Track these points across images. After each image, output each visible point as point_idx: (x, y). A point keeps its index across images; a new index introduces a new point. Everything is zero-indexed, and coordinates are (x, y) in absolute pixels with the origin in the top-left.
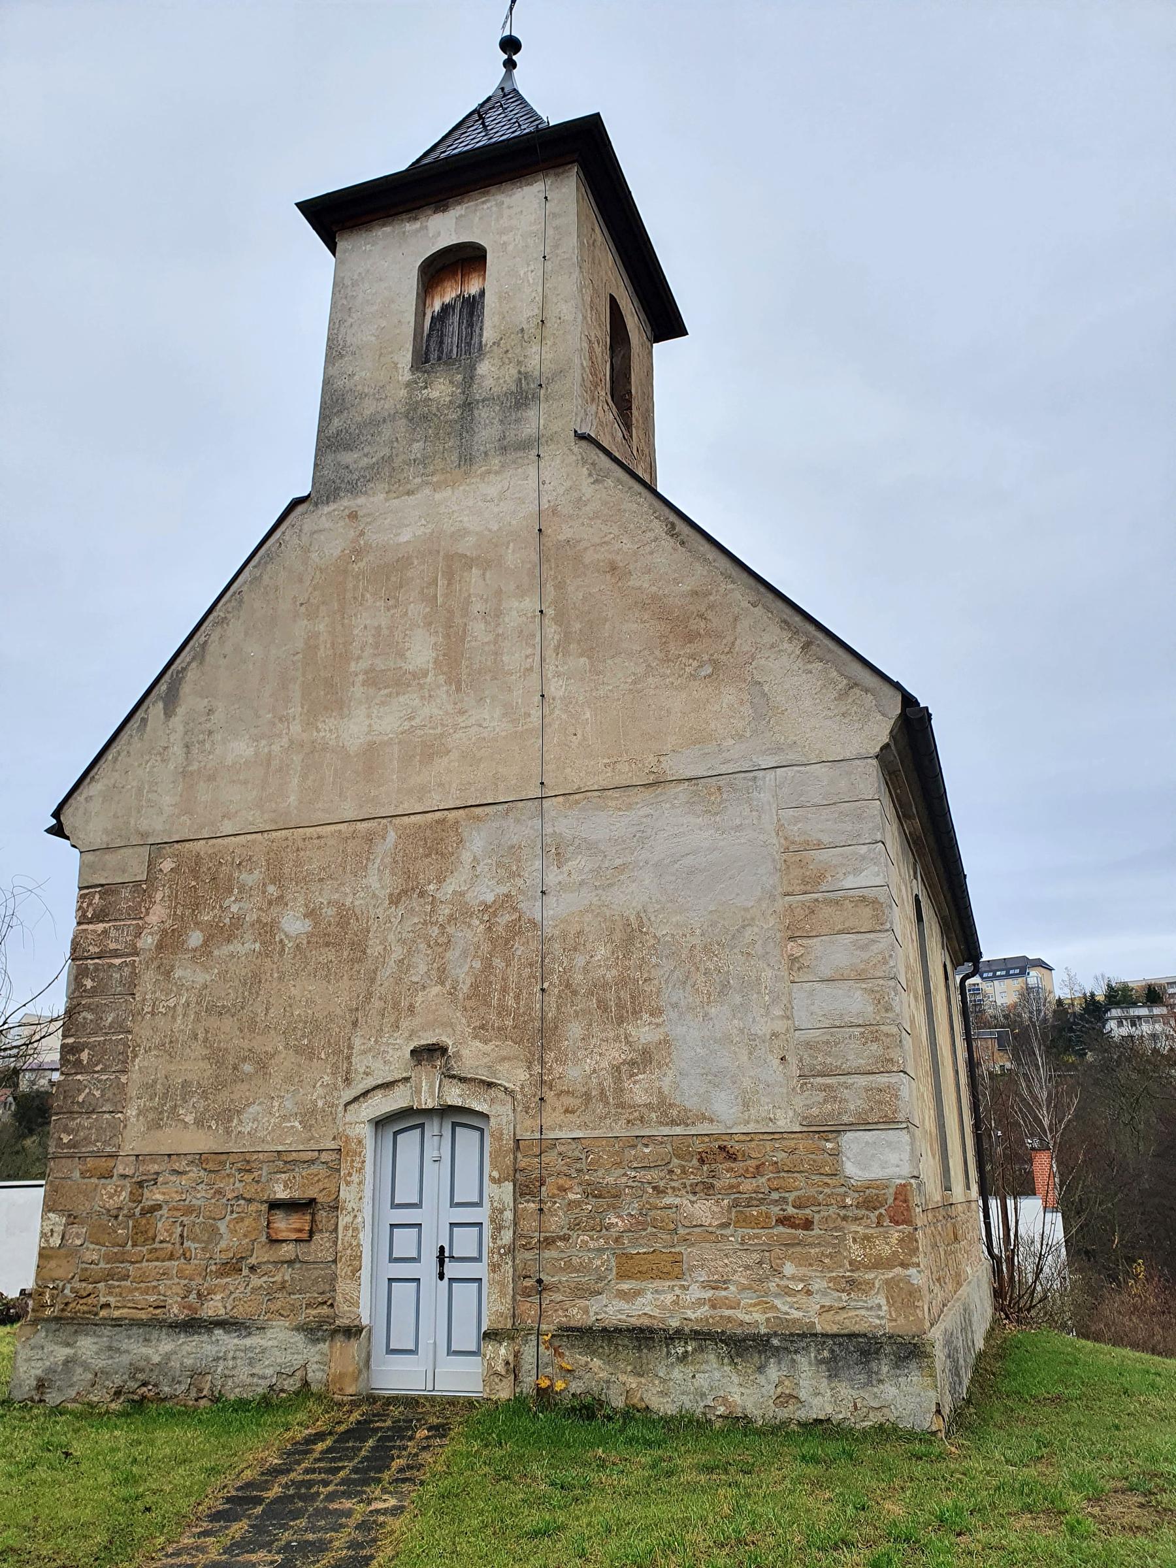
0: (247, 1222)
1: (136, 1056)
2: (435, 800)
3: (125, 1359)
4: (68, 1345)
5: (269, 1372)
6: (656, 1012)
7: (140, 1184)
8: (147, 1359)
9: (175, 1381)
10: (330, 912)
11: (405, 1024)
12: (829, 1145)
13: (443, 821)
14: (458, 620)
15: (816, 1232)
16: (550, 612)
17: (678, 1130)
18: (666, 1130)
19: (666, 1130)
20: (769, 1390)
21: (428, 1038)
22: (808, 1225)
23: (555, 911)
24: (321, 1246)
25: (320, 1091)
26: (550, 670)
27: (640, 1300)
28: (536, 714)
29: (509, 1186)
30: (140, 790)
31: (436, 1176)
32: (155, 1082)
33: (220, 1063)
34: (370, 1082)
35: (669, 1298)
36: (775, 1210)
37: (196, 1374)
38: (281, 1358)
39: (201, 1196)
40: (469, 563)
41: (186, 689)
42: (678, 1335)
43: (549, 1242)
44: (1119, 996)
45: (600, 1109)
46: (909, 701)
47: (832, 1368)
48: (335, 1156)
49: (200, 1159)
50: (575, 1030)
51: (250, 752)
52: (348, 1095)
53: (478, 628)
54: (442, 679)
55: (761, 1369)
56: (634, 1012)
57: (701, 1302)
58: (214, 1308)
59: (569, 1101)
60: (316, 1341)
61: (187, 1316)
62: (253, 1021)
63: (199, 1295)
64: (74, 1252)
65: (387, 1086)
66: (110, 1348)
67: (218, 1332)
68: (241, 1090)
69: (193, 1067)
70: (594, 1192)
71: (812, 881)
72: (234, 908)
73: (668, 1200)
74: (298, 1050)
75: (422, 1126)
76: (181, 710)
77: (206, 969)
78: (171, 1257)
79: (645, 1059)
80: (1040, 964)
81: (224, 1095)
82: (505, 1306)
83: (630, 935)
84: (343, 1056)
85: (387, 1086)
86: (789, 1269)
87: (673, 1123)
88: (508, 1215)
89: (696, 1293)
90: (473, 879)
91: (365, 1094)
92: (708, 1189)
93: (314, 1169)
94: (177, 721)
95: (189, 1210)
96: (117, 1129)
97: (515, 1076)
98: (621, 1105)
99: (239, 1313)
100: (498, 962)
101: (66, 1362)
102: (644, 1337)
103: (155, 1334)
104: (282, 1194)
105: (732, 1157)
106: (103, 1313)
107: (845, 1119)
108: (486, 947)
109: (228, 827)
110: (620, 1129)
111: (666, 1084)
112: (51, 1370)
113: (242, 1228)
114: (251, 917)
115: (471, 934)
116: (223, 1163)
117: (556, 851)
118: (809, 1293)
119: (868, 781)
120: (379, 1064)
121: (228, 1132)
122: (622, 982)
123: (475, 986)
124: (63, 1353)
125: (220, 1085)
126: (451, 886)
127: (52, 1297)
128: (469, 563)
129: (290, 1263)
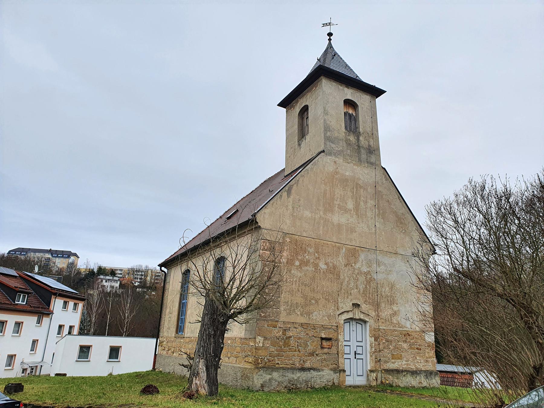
0: (315, 343)
1: (282, 293)
2: (354, 243)
3: (287, 378)
4: (270, 374)
5: (325, 381)
6: (397, 304)
7: (285, 330)
8: (293, 378)
9: (301, 384)
10: (331, 265)
11: (350, 297)
13: (355, 249)
14: (358, 200)
17: (401, 329)
18: (399, 329)
19: (399, 329)
20: (418, 381)
21: (355, 302)
22: (420, 349)
23: (380, 277)
24: (334, 350)
25: (331, 311)
28: (374, 229)
29: (373, 338)
30: (280, 216)
31: (353, 334)
32: (288, 301)
33: (306, 299)
34: (343, 310)
35: (400, 363)
37: (306, 382)
38: (327, 377)
39: (302, 335)
40: (361, 187)
41: (293, 191)
42: (402, 371)
43: (380, 351)
44: (102, 271)
45: (388, 323)
47: (426, 377)
49: (302, 325)
50: (383, 305)
51: (310, 215)
52: (339, 313)
53: (362, 203)
54: (355, 213)
55: (416, 377)
57: (405, 364)
58: (308, 365)
59: (382, 320)
60: (336, 373)
62: (314, 290)
63: (304, 361)
64: (266, 349)
65: (348, 312)
66: (283, 375)
67: (312, 371)
68: (312, 307)
69: (299, 299)
70: (387, 341)
72: (307, 257)
73: (400, 343)
74: (326, 299)
75: (349, 322)
76: (292, 197)
77: (301, 272)
78: (295, 351)
80: (75, 255)
81: (308, 308)
82: (373, 365)
84: (336, 302)
85: (348, 312)
87: (400, 328)
88: (373, 345)
89: (404, 362)
90: (361, 265)
91: (343, 313)
93: (330, 330)
94: (291, 199)
95: (300, 338)
96: (278, 314)
97: (373, 314)
98: (392, 323)
99: (315, 366)
100: (368, 286)
101: (270, 380)
102: (397, 371)
103: (295, 371)
104: (324, 336)
105: (409, 335)
106: (277, 366)
108: (365, 282)
110: (392, 328)
111: (399, 319)
113: (314, 344)
114: (312, 261)
115: (362, 279)
116: (308, 326)
117: (378, 264)
120: (344, 306)
121: (309, 318)
122: (391, 296)
123: (364, 291)
124: (269, 377)
125: (306, 305)
126: (358, 266)
127: (261, 361)
128: (361, 187)
129: (326, 354)
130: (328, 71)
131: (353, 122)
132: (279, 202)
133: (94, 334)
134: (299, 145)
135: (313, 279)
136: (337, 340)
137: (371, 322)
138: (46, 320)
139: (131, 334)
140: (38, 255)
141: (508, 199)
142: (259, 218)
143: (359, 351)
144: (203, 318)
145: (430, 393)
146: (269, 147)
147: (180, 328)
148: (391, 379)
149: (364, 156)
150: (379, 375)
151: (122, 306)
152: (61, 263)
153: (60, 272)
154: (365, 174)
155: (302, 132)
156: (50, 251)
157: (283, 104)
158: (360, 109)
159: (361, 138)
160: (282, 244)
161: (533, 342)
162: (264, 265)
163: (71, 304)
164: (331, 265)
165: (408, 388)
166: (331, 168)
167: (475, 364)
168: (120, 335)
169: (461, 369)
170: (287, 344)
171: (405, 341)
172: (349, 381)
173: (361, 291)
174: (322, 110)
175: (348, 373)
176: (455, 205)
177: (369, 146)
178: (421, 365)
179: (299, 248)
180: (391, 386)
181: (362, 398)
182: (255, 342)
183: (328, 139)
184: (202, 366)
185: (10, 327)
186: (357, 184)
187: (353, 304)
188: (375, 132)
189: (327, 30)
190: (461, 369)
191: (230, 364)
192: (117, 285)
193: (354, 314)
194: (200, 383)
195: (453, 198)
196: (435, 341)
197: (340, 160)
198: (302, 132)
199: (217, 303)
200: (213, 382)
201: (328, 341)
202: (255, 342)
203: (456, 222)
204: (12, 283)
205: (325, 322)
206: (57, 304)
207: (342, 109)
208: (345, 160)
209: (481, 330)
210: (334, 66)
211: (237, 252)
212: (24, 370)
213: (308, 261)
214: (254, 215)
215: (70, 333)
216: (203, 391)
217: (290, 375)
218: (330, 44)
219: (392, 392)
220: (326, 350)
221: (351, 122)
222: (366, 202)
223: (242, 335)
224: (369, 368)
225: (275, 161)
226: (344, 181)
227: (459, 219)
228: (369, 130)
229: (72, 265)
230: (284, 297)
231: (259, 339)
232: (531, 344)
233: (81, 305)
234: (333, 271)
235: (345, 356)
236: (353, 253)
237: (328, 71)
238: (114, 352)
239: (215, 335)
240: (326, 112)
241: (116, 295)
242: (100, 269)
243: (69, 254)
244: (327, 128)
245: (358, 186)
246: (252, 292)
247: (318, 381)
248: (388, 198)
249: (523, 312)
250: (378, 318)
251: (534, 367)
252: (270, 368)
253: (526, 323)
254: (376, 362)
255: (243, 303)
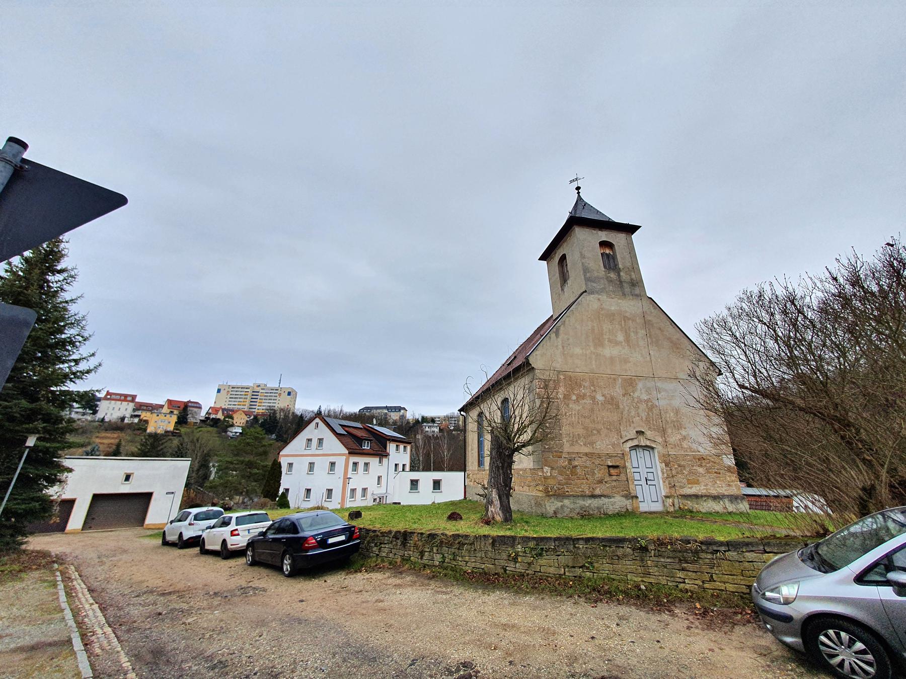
2: (629, 373)
10: (608, 396)
23: (662, 403)
31: (641, 461)
33: (587, 430)
37: (598, 508)
40: (629, 319)
41: (561, 332)
42: (702, 496)
44: (424, 419)
47: (731, 501)
49: (586, 454)
50: (670, 431)
53: (632, 334)
58: (597, 492)
64: (554, 478)
65: (632, 439)
68: (594, 438)
70: (679, 466)
79: (684, 438)
80: (404, 409)
81: (590, 438)
84: (619, 432)
85: (632, 439)
90: (640, 393)
94: (559, 339)
95: (586, 467)
96: (562, 446)
97: (659, 440)
99: (605, 493)
102: (696, 496)
104: (610, 464)
109: (578, 370)
112: (557, 508)
115: (643, 406)
117: (658, 390)
126: (636, 395)
128: (629, 319)
130: (581, 220)
131: (611, 261)
132: (548, 344)
133: (424, 470)
134: (563, 290)
135: (592, 410)
136: (625, 467)
137: (659, 448)
138: (385, 460)
139: (451, 469)
140: (379, 411)
141: (793, 303)
142: (532, 360)
143: (650, 477)
144: (491, 452)
145: (737, 518)
146: (533, 296)
147: (480, 463)
148: (689, 504)
149: (627, 289)
150: (676, 501)
151: (436, 447)
152: (395, 416)
153: (395, 423)
154: (630, 306)
155: (564, 278)
156: (386, 408)
157: (543, 258)
158: (616, 247)
159: (622, 274)
160: (557, 383)
161: (858, 461)
162: (542, 402)
163: (402, 447)
164: (608, 396)
165: (711, 514)
166: (595, 305)
167: (791, 487)
168: (442, 470)
169: (764, 492)
170: (573, 473)
171: (701, 466)
172: (644, 507)
173: (644, 418)
174: (579, 255)
175: (641, 499)
176: (730, 319)
177: (632, 279)
178: (723, 490)
179: (573, 383)
180: (691, 512)
181: (656, 524)
182: (543, 472)
183: (587, 280)
184: (495, 495)
185: (361, 467)
186: (625, 317)
187: (637, 432)
188: (635, 266)
189: (575, 185)
190: (764, 492)
191: (523, 493)
192: (437, 430)
193: (639, 441)
194: (495, 510)
195: (725, 313)
196: (736, 464)
197: (604, 297)
198: (564, 278)
199: (502, 439)
200: (506, 509)
201: (616, 468)
202: (543, 472)
203: (733, 335)
204: (360, 434)
205: (610, 451)
206: (391, 447)
207: (599, 251)
208: (609, 296)
209: (783, 450)
210: (585, 215)
211: (516, 392)
212: (375, 500)
213: (585, 395)
214: (527, 358)
215: (403, 470)
216: (499, 518)
217: (581, 502)
218: (579, 196)
219: (692, 518)
220: (614, 478)
221: (610, 261)
222: (637, 333)
223: (531, 466)
224: (664, 494)
225: (548, 312)
226: (611, 316)
227: (738, 335)
228: (629, 264)
229: (403, 417)
230: (565, 429)
231: (546, 469)
232: (854, 461)
233: (409, 448)
234: (612, 402)
235: (636, 483)
236: (630, 383)
237: (581, 220)
238: (437, 484)
239: (503, 467)
240: (583, 256)
241: (437, 438)
242: (423, 418)
243: (399, 409)
244: (586, 270)
245: (626, 319)
246: (534, 426)
247: (611, 507)
248: (659, 325)
249: (837, 426)
250: (666, 444)
251: (864, 489)
252: (560, 495)
253: (843, 438)
254: (670, 488)
255: (525, 437)
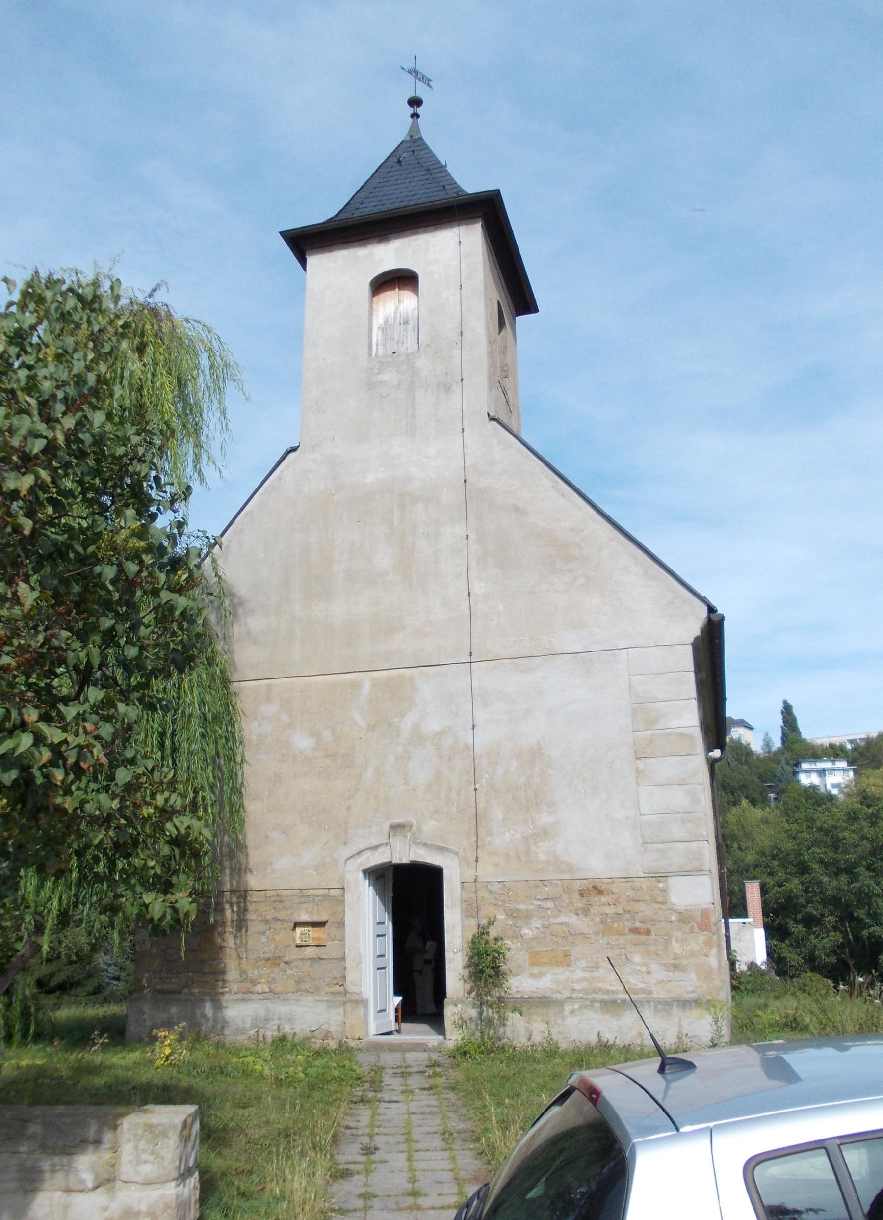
12: (661, 885)
15: (653, 937)
16: (472, 536)
22: (648, 932)
26: (473, 573)
27: (544, 979)
36: (628, 925)
46: (711, 610)
48: (339, 892)
56: (537, 804)
61: (727, 1009)
71: (650, 723)
83: (536, 755)
85: (376, 848)
86: (637, 959)
91: (359, 853)
92: (586, 912)
105: (600, 892)
107: (671, 870)
118: (649, 973)
119: (686, 660)
